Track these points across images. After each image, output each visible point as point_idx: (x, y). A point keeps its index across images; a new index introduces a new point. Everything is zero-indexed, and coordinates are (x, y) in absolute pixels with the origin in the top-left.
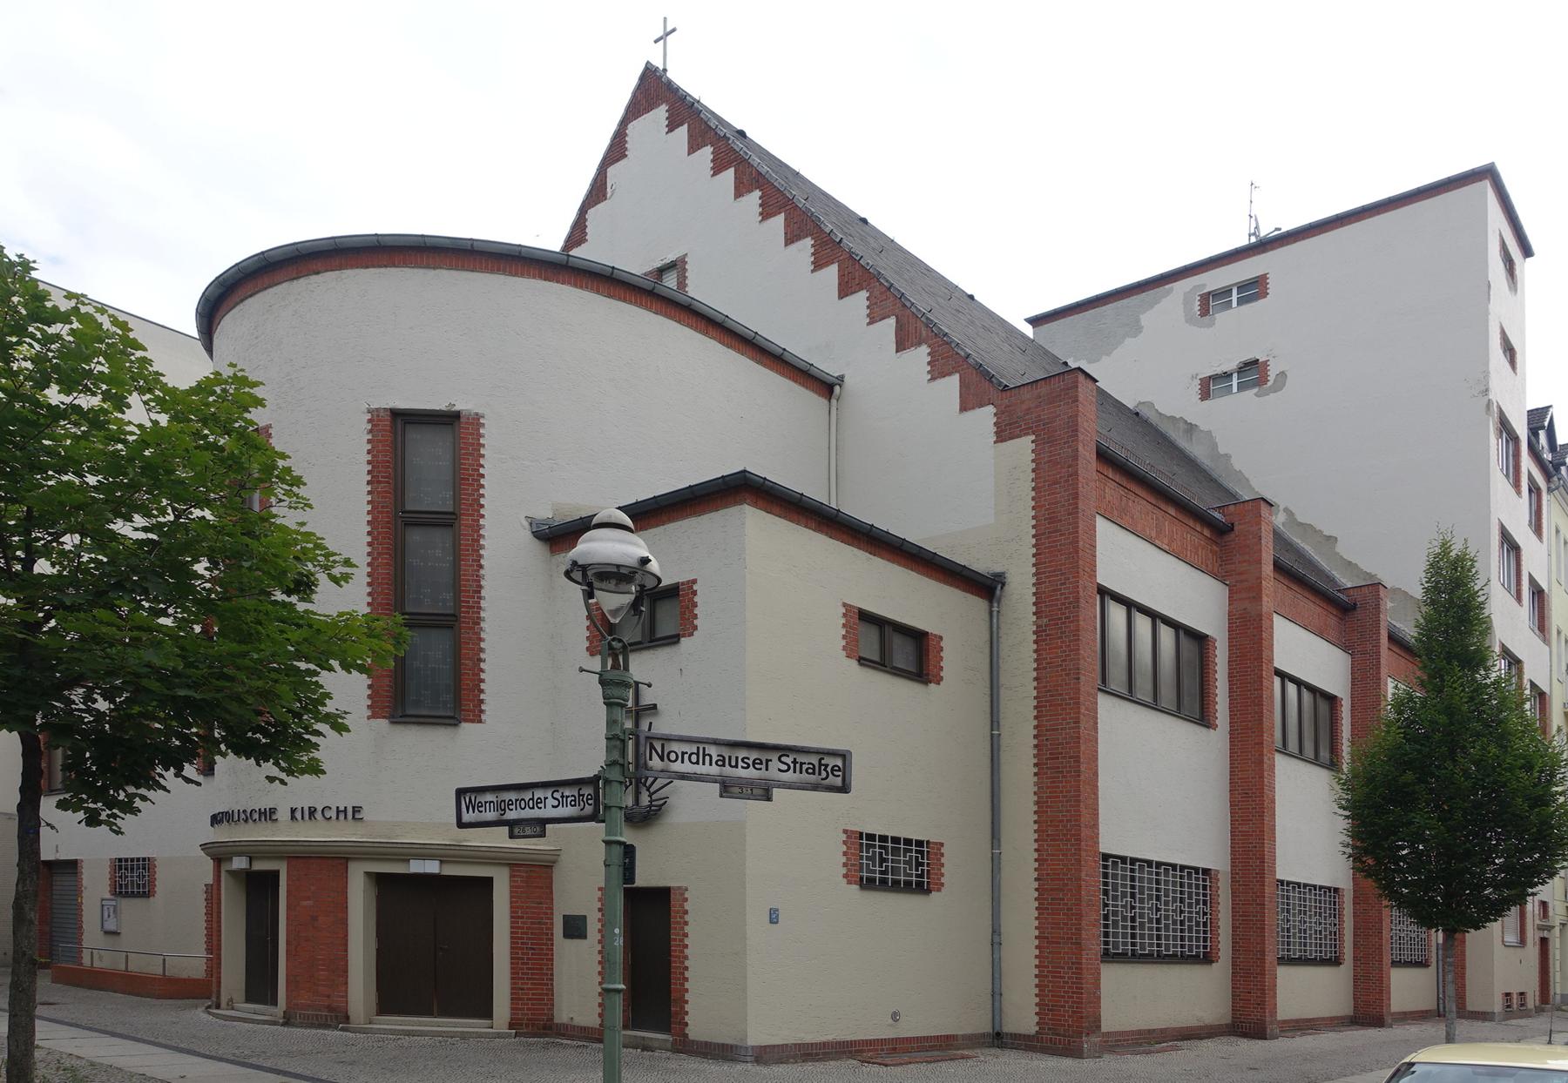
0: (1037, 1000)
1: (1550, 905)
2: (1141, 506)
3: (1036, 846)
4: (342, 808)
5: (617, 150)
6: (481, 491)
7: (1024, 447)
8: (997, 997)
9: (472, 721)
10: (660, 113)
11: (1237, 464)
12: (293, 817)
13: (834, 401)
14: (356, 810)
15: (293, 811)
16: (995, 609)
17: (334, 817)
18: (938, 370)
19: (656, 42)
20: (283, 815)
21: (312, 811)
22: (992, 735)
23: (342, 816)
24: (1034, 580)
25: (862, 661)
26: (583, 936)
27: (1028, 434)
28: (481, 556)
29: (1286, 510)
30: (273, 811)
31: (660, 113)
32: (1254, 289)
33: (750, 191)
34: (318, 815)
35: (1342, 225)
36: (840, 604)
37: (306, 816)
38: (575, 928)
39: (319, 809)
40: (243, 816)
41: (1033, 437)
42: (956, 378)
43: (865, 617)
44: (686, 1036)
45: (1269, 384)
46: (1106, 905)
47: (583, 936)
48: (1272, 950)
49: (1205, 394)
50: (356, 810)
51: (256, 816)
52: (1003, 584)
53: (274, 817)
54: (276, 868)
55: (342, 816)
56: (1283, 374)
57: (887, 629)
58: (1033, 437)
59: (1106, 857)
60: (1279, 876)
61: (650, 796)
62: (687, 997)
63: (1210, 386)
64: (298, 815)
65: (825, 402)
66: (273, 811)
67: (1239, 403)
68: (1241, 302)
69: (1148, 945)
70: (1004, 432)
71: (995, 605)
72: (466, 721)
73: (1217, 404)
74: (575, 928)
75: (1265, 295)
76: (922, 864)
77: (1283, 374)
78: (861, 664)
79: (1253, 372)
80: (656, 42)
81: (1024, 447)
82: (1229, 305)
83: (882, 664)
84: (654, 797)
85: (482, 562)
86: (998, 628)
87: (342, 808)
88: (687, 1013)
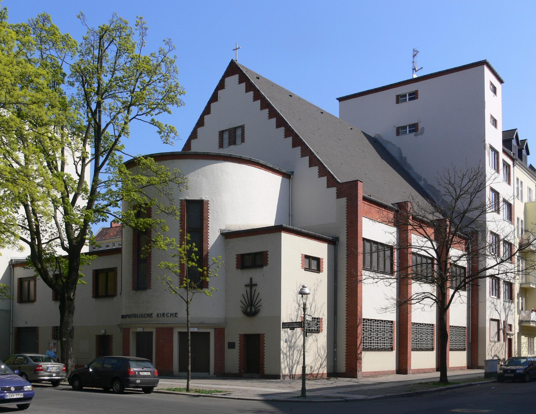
0: (346, 362)
1: (513, 326)
2: (374, 209)
3: (346, 318)
4: (172, 313)
5: (221, 85)
6: (208, 222)
7: (344, 200)
8: (335, 362)
9: (206, 288)
10: (236, 77)
11: (409, 161)
12: (158, 316)
13: (291, 180)
14: (176, 314)
15: (158, 314)
16: (336, 248)
17: (170, 316)
18: (321, 175)
19: (233, 50)
20: (155, 315)
21: (164, 314)
22: (335, 285)
23: (172, 316)
24: (346, 240)
25: (306, 269)
26: (234, 348)
27: (345, 197)
28: (208, 241)
29: (424, 179)
30: (151, 314)
31: (236, 77)
32: (414, 96)
33: (265, 109)
34: (165, 315)
35: (441, 75)
36: (300, 254)
37: (162, 315)
38: (232, 345)
39: (166, 314)
40: (141, 316)
41: (346, 198)
42: (326, 177)
43: (307, 257)
44: (264, 373)
45: (419, 131)
46: (363, 334)
47: (234, 348)
48: (410, 346)
49: (398, 134)
50: (176, 314)
51: (146, 316)
52: (338, 241)
53: (152, 316)
54: (152, 331)
55: (172, 316)
56: (423, 128)
57: (311, 259)
58: (346, 198)
59: (364, 319)
60: (413, 321)
61: (255, 309)
62: (264, 363)
63: (400, 130)
64: (159, 315)
65: (288, 180)
66: (151, 314)
67: (409, 137)
68: (410, 99)
69: (375, 346)
70: (339, 196)
71: (336, 246)
72: (204, 288)
73: (402, 137)
74: (232, 345)
75: (417, 98)
76: (318, 325)
77: (423, 128)
78: (305, 270)
79: (414, 128)
80: (233, 50)
81: (344, 200)
82: (405, 100)
83: (308, 269)
84: (256, 309)
85: (209, 242)
86: (337, 253)
87: (172, 313)
88: (264, 367)
